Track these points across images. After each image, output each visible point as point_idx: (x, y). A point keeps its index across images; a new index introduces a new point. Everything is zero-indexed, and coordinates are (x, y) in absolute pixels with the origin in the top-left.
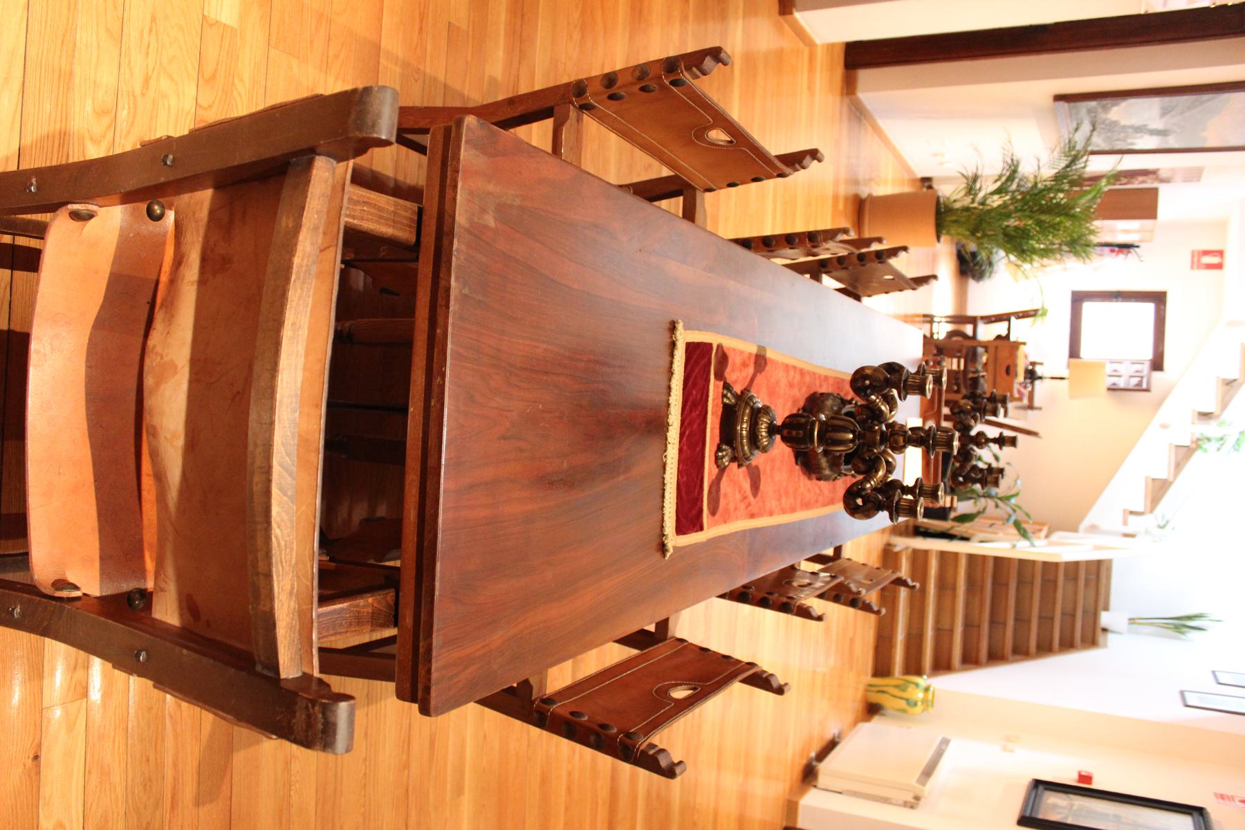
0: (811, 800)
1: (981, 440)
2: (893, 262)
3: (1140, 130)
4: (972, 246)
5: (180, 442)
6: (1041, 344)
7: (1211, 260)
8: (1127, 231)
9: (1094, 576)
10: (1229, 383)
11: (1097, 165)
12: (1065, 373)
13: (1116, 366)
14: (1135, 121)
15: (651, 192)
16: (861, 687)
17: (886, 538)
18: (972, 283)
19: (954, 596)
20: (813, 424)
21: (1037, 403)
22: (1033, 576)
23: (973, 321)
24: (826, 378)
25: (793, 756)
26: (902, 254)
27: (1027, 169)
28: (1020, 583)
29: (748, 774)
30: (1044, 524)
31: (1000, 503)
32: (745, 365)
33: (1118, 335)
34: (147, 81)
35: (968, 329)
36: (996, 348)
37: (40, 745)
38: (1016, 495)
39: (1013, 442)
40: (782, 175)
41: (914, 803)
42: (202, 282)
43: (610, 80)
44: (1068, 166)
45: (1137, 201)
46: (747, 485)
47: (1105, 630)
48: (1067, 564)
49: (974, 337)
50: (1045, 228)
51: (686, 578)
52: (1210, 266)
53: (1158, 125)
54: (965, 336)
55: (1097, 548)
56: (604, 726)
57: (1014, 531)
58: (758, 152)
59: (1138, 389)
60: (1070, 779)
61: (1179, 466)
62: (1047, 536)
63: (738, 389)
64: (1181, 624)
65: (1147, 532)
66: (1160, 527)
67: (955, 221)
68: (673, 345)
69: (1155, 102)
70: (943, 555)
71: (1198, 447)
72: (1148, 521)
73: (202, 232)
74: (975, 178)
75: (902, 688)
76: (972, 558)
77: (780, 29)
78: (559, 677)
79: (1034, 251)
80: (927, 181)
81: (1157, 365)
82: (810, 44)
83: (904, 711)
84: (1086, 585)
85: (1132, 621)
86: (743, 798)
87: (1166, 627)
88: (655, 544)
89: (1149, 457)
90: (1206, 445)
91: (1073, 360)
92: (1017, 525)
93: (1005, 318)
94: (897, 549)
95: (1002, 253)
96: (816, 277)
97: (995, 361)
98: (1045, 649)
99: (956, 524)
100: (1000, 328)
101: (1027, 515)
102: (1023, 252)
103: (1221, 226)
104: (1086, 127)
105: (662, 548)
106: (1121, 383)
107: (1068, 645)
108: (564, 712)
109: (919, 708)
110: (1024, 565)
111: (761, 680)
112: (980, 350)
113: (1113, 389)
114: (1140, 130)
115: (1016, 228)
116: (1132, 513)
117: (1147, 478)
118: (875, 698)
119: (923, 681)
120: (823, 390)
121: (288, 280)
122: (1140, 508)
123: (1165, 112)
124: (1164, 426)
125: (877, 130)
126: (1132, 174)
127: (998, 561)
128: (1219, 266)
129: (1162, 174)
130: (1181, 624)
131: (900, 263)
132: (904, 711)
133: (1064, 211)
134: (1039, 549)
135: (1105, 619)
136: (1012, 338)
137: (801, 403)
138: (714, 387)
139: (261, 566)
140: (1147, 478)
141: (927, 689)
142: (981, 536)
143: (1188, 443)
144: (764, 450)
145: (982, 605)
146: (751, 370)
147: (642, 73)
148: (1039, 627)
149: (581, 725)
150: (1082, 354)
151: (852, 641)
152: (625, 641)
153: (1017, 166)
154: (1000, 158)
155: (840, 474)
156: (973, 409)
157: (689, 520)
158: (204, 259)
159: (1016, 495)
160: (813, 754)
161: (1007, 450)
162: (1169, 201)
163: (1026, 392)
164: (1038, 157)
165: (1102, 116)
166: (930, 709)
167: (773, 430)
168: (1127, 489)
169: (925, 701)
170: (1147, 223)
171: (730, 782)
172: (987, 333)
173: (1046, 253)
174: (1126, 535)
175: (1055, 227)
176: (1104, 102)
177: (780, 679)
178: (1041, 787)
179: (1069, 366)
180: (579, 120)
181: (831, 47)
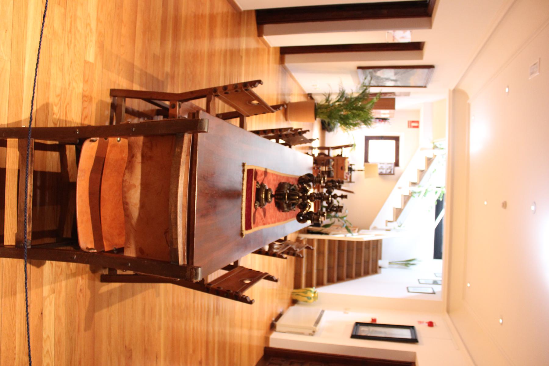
0: (274, 336)
1: (335, 196)
2: (304, 135)
3: (387, 79)
4: (327, 121)
5: (138, 206)
6: (354, 158)
7: (414, 124)
8: (385, 114)
9: (376, 245)
10: (422, 171)
11: (373, 90)
12: (363, 168)
13: (382, 165)
15: (226, 117)
16: (290, 293)
17: (297, 235)
19: (324, 256)
20: (285, 194)
21: (353, 180)
22: (353, 248)
23: (328, 149)
24: (284, 177)
25: (266, 319)
26: (308, 133)
28: (349, 250)
29: (251, 328)
30: (356, 227)
31: (340, 220)
32: (262, 175)
33: (381, 153)
34: (69, 84)
35: (326, 152)
36: (337, 160)
37: (42, 310)
38: (346, 216)
39: (346, 197)
40: (273, 112)
41: (313, 333)
42: (143, 162)
43: (225, 88)
45: (388, 103)
46: (262, 214)
47: (380, 267)
48: (366, 242)
49: (329, 155)
50: (355, 116)
51: (244, 245)
52: (414, 127)
53: (394, 78)
54: (325, 155)
55: (376, 235)
56: (228, 291)
57: (346, 230)
58: (266, 106)
59: (390, 174)
60: (368, 320)
61: (405, 203)
62: (358, 232)
63: (260, 183)
64: (407, 263)
65: (394, 229)
66: (399, 226)
67: (322, 113)
68: (244, 171)
69: (392, 71)
70: (319, 241)
71: (412, 195)
72: (395, 224)
73: (141, 149)
74: (329, 95)
75: (305, 292)
76: (330, 241)
77: (258, 42)
78: (212, 278)
79: (351, 124)
80: (310, 96)
81: (397, 164)
82: (269, 47)
83: (306, 301)
84: (373, 250)
85: (390, 263)
86: (250, 337)
87: (402, 264)
88: (239, 232)
89: (394, 200)
90: (414, 195)
91: (366, 164)
92: (347, 228)
93: (340, 147)
94: (301, 239)
95: (339, 124)
97: (337, 164)
98: (358, 275)
99: (323, 228)
100: (338, 152)
101: (350, 224)
103: (418, 112)
104: (369, 78)
105: (242, 235)
106: (384, 172)
107: (367, 273)
108: (216, 287)
109: (312, 300)
110: (350, 243)
111: (270, 278)
112: (331, 160)
113: (381, 174)
114: (387, 79)
115: (344, 115)
116: (389, 221)
117: (394, 208)
118: (295, 297)
119: (313, 289)
121: (180, 165)
122: (392, 219)
123: (396, 74)
124: (400, 188)
125: (292, 77)
126: (386, 94)
127: (340, 242)
128: (417, 127)
129: (397, 94)
130: (407, 263)
131: (306, 136)
132: (306, 301)
133: (362, 109)
134: (355, 237)
135: (380, 263)
136: (343, 156)
137: (277, 186)
138: (254, 182)
139: (174, 237)
141: (315, 293)
142: (333, 232)
143: (408, 194)
144: (269, 202)
145: (334, 259)
146: (263, 176)
147: (236, 87)
148: (356, 266)
149: (221, 291)
151: (286, 275)
152: (224, 269)
155: (290, 210)
156: (333, 186)
157: (248, 227)
158: (143, 156)
159: (346, 216)
160: (274, 319)
161: (344, 199)
162: (399, 103)
163: (348, 176)
165: (374, 74)
166: (317, 301)
167: (272, 196)
168: (387, 213)
169: (314, 297)
170: (392, 111)
171: (245, 332)
172: (333, 153)
173: (355, 125)
174: (387, 230)
175: (359, 115)
176: (376, 70)
177: (276, 277)
178: (358, 325)
179: (364, 165)
180: (214, 99)
181: (275, 48)
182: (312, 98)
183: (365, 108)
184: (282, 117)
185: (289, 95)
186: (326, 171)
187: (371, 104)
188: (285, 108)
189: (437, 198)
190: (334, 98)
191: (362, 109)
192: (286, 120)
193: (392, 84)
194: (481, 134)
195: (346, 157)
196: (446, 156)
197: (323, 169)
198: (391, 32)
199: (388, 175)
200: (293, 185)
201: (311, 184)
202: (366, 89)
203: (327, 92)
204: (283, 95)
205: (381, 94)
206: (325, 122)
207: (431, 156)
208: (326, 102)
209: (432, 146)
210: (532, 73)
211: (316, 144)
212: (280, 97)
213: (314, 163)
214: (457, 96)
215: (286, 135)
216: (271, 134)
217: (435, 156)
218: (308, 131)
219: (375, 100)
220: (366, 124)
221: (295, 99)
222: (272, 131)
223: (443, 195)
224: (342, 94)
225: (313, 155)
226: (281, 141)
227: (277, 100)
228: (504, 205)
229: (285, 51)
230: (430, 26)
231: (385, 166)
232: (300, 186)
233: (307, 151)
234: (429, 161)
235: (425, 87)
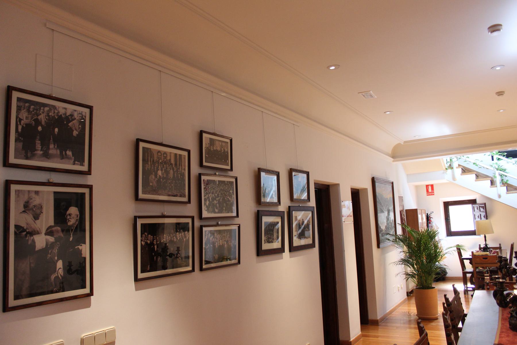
2: (450, 300)
3: (388, 219)
6: (471, 245)
7: (430, 189)
8: (422, 218)
11: (399, 232)
14: (385, 221)
18: (448, 275)
21: (498, 246)
23: (465, 274)
24: (502, 324)
27: (402, 256)
33: (463, 218)
35: (469, 275)
40: (427, 334)
44: (402, 241)
50: (426, 248)
67: (426, 281)
69: (379, 215)
71: (506, 183)
79: (436, 251)
80: (409, 294)
81: (473, 202)
93: (462, 261)
95: (437, 263)
96: (460, 330)
100: (467, 263)
102: (436, 255)
103: (417, 187)
104: (388, 236)
106: (483, 214)
112: (477, 270)
113: (486, 217)
114: (388, 219)
120: (508, 325)
124: (500, 196)
128: (432, 186)
129: (401, 209)
133: (419, 241)
136: (471, 257)
140: (290, 257)
143: (505, 187)
150: (473, 229)
153: (402, 259)
154: (400, 266)
162: (411, 204)
163: (493, 251)
164: (396, 254)
170: (419, 211)
172: (469, 268)
173: (436, 247)
175: (426, 244)
181: (362, 329)
182: (412, 292)
183: (418, 239)
184: (433, 324)
185: (409, 315)
186: (490, 276)
187: (413, 233)
188: (424, 319)
189: (504, 158)
190: (410, 270)
191: (419, 241)
192: (437, 319)
193: (392, 214)
194: (431, 128)
195: (471, 254)
196: (458, 156)
197: (487, 278)
198: (343, 218)
199: (484, 208)
200: (511, 314)
201: (505, 293)
202: (399, 239)
203: (404, 276)
204: (410, 322)
205: (402, 223)
206: (435, 278)
207: (460, 170)
208: (415, 277)
209: (450, 171)
210: (371, 96)
211: (460, 287)
212: (413, 326)
213: (483, 289)
214: (398, 153)
215: (452, 320)
216: (453, 337)
217: (459, 165)
218: (445, 296)
219: (408, 229)
220: (435, 236)
221: (414, 310)
222: (448, 336)
223: (499, 152)
224: (405, 261)
225: (474, 290)
226: (460, 325)
227: (415, 328)
228: (500, 93)
229: (366, 320)
230: (337, 185)
231: (477, 213)
232: (511, 305)
233: (470, 296)
234: (465, 171)
235: (392, 183)
